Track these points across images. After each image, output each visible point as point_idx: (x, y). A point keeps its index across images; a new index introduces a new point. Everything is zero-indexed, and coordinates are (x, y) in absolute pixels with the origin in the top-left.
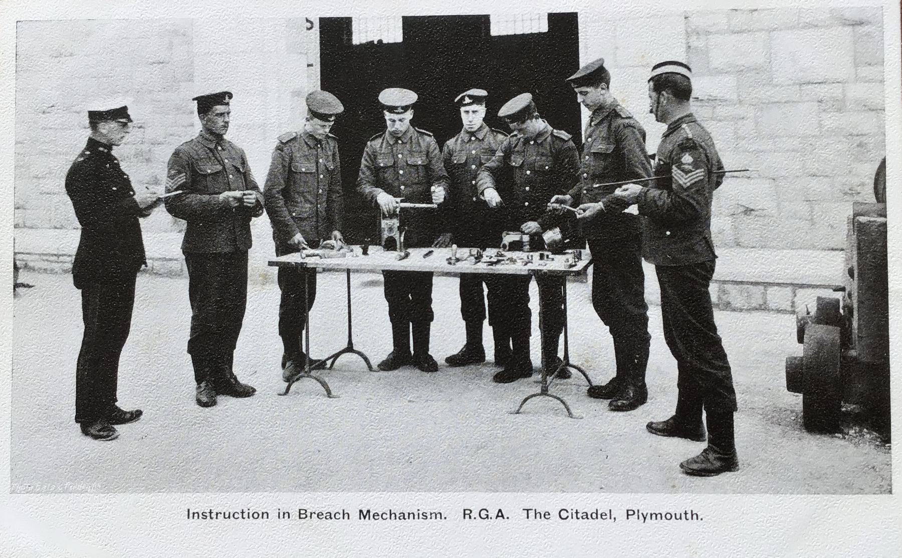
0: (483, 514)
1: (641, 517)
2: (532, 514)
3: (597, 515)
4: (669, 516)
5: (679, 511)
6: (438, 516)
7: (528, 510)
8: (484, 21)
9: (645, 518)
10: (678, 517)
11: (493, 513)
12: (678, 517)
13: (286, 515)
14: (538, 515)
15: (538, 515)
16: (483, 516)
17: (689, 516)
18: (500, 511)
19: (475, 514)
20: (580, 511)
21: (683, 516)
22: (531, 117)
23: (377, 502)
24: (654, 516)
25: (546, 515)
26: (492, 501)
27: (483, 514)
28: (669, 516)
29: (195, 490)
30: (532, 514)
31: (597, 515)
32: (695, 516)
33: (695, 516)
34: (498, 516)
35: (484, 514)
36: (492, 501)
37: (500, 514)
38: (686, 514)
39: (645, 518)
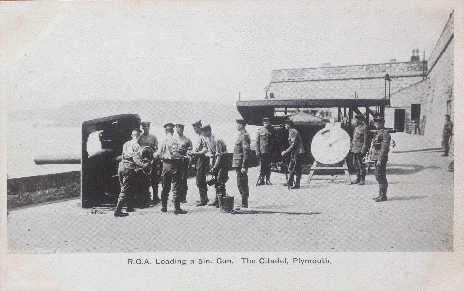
0: (138, 261)
1: (301, 261)
2: (246, 261)
3: (279, 261)
4: (314, 261)
5: (320, 258)
6: (229, 261)
7: (244, 259)
8: (85, 206)
9: (303, 263)
10: (319, 262)
11: (143, 261)
12: (319, 262)
13: (229, 261)
14: (249, 261)
15: (249, 261)
16: (138, 262)
17: (325, 261)
18: (147, 260)
19: (134, 261)
20: (270, 259)
21: (322, 261)
22: (218, 192)
23: (304, 255)
24: (307, 261)
25: (253, 261)
26: (143, 256)
27: (138, 261)
28: (314, 261)
29: (287, 251)
30: (246, 261)
31: (279, 261)
32: (327, 261)
33: (327, 261)
34: (145, 262)
35: (139, 262)
36: (143, 256)
37: (147, 261)
38: (323, 260)
39: (303, 263)
